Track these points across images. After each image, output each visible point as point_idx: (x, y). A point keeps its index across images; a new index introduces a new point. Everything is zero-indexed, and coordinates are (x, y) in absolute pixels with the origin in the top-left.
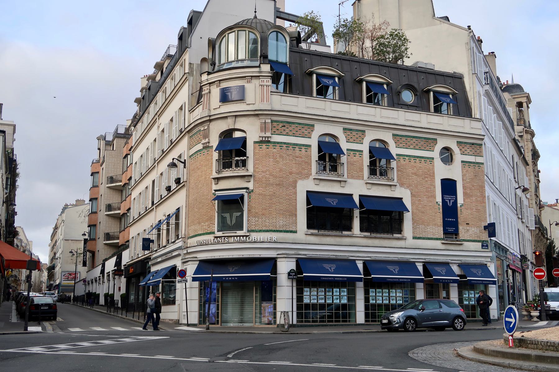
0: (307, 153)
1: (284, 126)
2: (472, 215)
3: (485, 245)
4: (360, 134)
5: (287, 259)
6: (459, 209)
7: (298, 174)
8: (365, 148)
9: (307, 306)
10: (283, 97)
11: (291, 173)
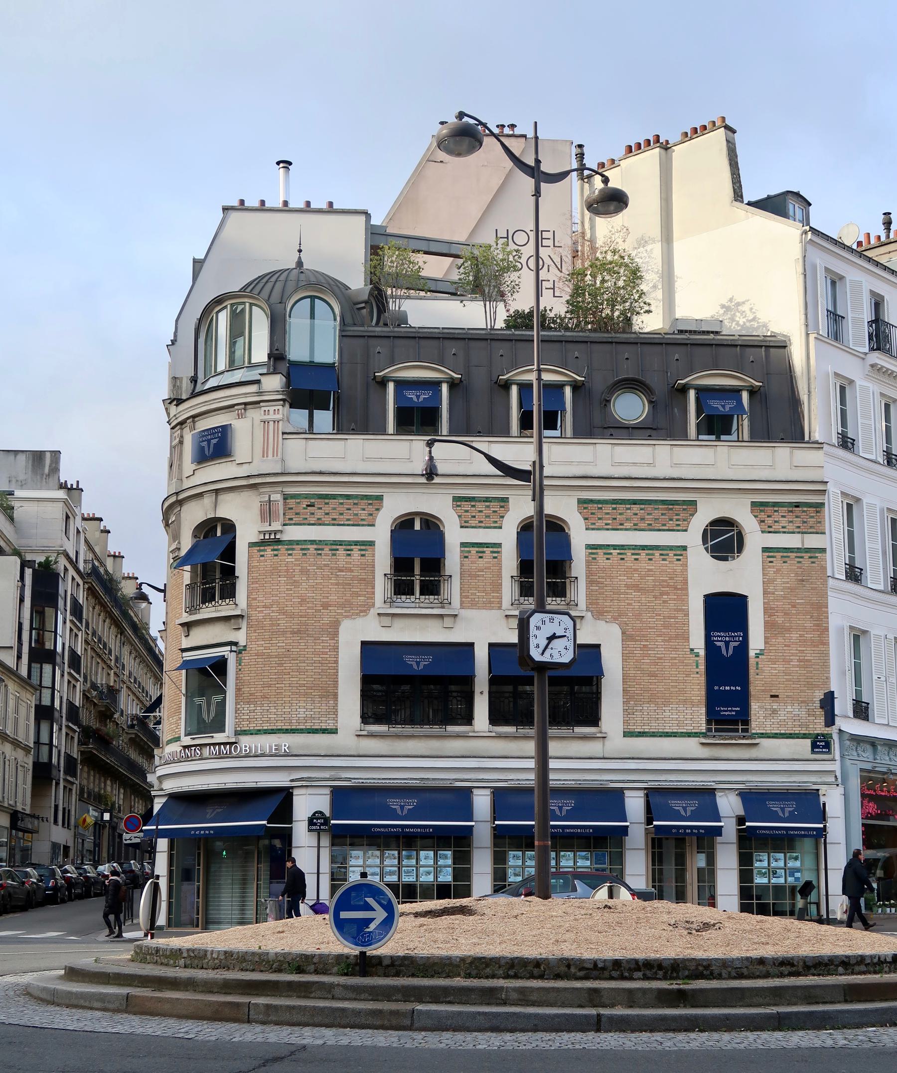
0: (363, 560)
1: (312, 505)
2: (786, 674)
3: (820, 744)
4: (495, 506)
5: (310, 791)
7: (342, 606)
8: (381, 534)
10: (310, 442)
11: (326, 606)
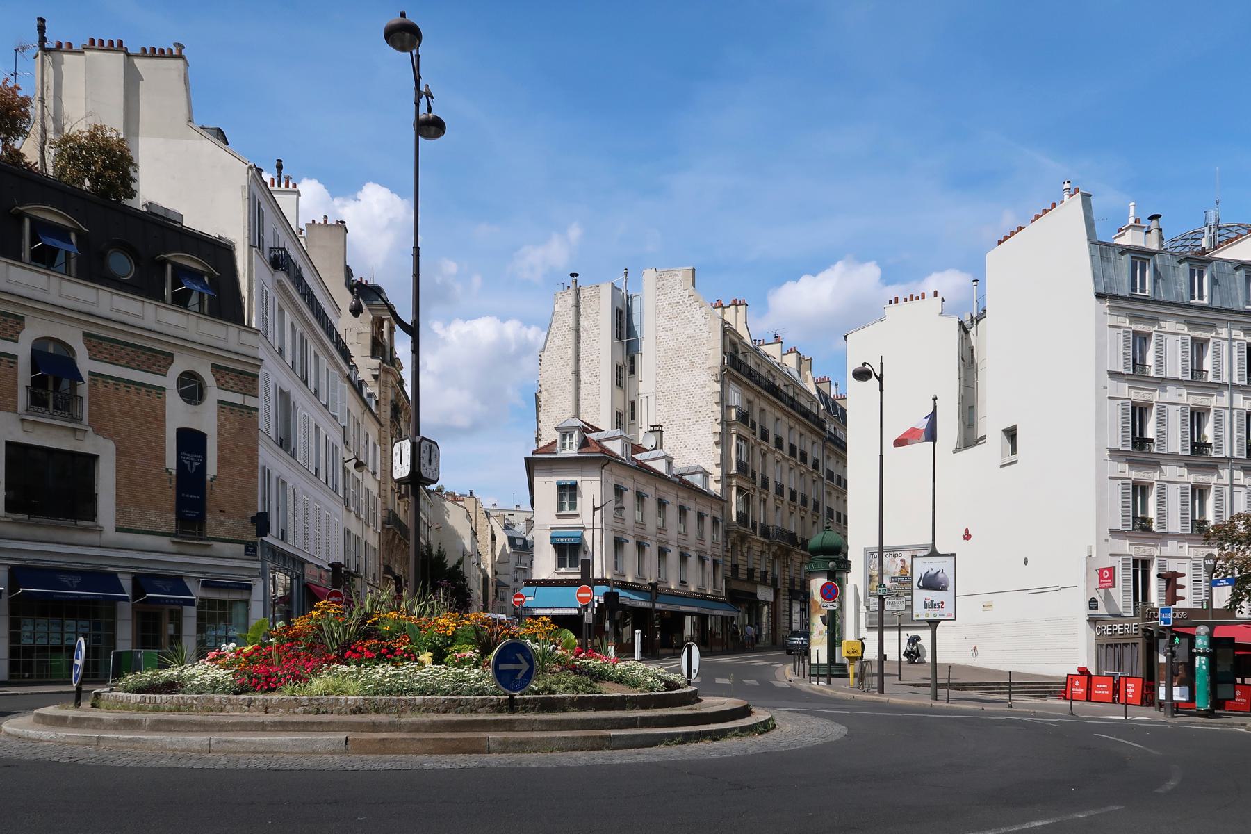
3: (250, 549)
4: (12, 322)
6: (208, 484)
8: (22, 349)
9: (28, 651)
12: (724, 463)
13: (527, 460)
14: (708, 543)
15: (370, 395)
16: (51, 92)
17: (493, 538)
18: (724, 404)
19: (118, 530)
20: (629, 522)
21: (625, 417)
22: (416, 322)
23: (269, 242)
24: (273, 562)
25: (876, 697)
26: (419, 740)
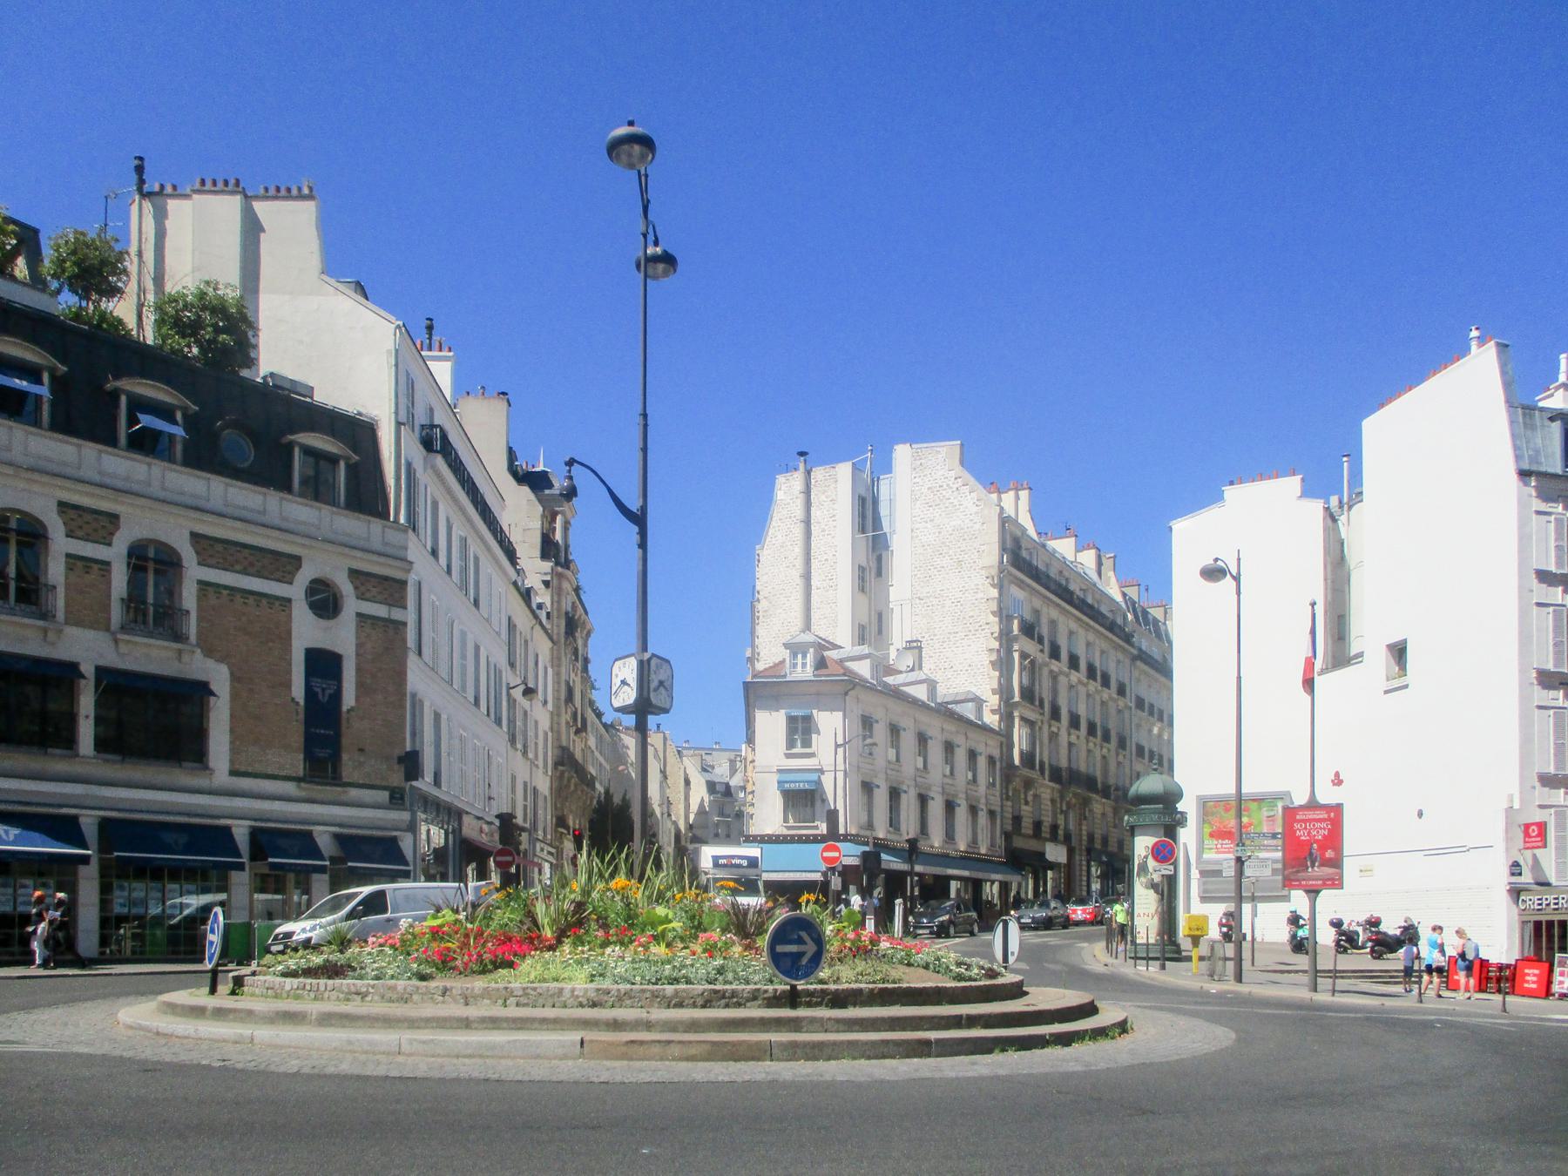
6: (344, 716)
12: (1004, 691)
13: (746, 685)
14: (982, 788)
15: (540, 606)
16: (152, 241)
17: (687, 782)
18: (1004, 615)
19: (234, 773)
20: (880, 763)
21: (872, 628)
22: (644, 509)
23: (421, 418)
24: (425, 812)
25: (1230, 986)
26: (680, 1042)
